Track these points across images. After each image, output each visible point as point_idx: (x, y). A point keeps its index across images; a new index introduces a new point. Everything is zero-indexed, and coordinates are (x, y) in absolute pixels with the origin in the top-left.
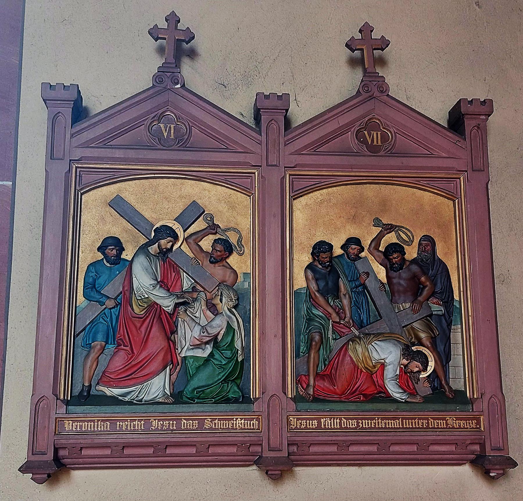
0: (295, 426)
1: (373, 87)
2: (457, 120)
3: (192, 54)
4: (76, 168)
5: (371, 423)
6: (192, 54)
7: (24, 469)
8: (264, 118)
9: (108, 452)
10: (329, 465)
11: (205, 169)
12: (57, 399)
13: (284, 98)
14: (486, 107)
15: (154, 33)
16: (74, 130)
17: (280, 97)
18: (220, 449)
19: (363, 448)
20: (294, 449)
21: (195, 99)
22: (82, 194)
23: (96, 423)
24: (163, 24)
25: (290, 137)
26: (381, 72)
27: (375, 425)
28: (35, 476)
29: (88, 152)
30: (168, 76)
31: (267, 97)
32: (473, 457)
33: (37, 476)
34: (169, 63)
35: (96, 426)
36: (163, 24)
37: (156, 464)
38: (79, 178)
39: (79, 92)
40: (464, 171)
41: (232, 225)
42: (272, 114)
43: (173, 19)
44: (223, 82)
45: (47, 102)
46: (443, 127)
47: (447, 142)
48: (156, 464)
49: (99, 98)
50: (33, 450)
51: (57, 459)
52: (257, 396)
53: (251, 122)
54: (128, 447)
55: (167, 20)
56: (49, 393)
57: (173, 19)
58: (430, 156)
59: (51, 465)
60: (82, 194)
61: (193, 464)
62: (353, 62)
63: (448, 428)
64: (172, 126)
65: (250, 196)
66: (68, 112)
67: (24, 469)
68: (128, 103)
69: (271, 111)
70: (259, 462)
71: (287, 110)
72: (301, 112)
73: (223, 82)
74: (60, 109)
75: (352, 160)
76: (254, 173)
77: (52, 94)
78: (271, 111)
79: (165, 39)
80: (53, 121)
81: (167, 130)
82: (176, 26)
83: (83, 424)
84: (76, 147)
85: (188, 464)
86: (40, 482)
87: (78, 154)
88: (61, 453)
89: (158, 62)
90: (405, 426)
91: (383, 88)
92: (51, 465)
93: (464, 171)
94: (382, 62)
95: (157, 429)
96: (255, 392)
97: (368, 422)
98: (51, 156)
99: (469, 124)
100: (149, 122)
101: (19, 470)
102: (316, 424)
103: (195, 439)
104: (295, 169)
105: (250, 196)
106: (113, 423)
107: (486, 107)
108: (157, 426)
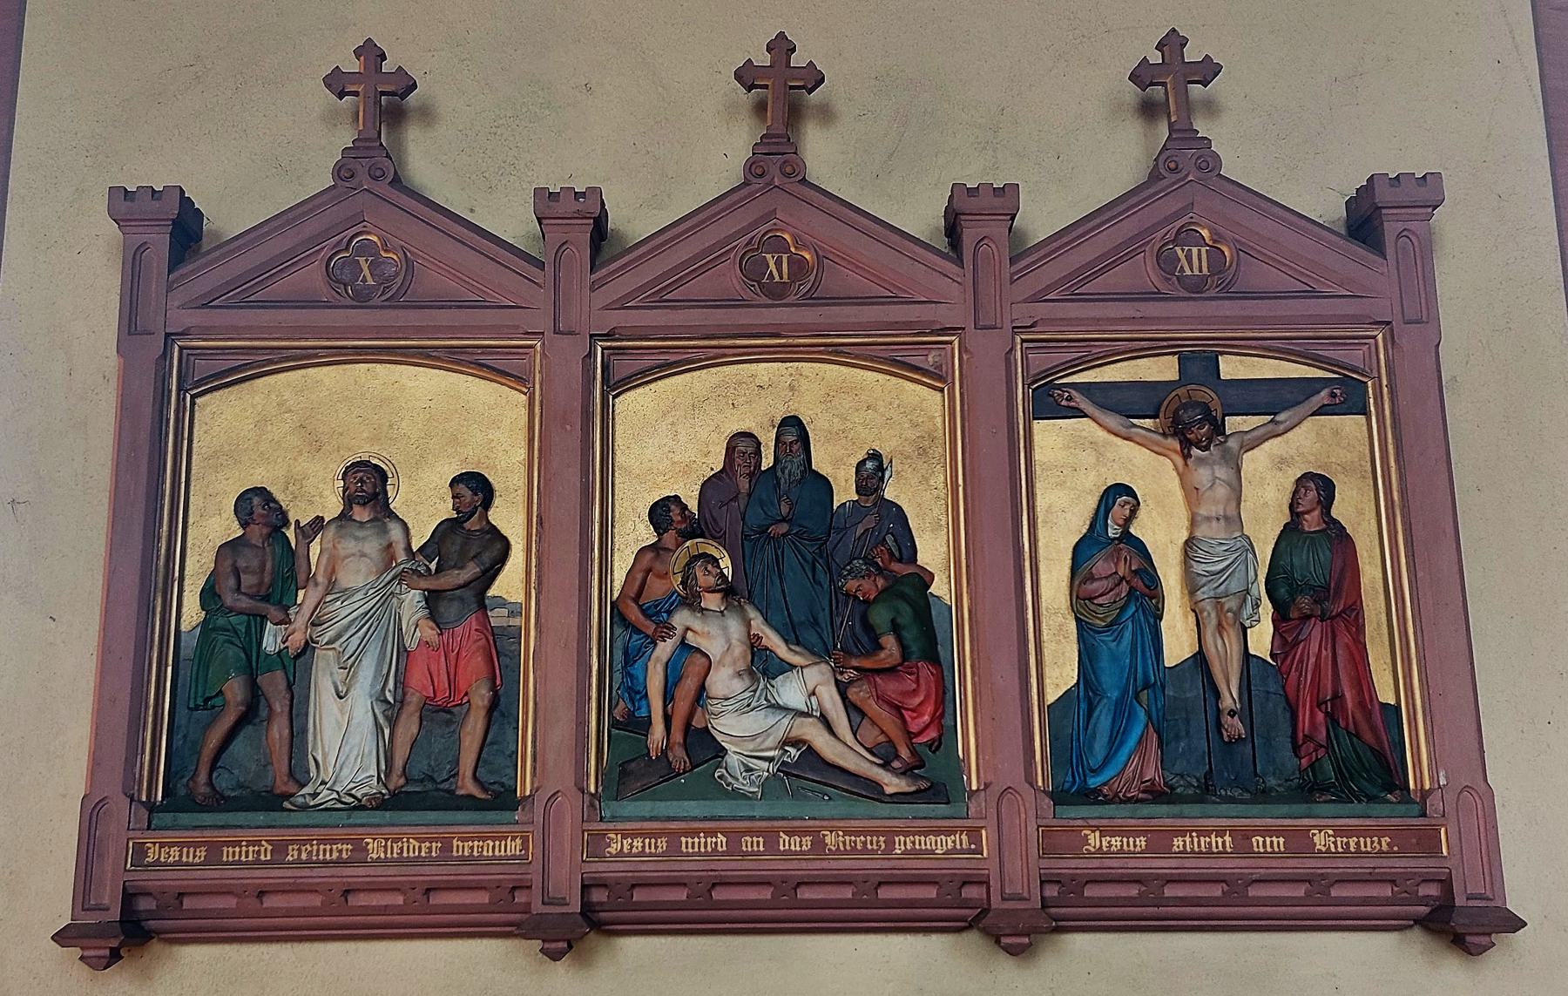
1: (1184, 161)
4: (181, 349)
7: (61, 937)
8: (969, 236)
9: (847, 893)
10: (278, 940)
12: (132, 800)
13: (1009, 192)
14: (1424, 194)
15: (337, 83)
16: (1014, 269)
17: (999, 192)
20: (1052, 891)
21: (835, 206)
26: (1202, 127)
28: (87, 953)
29: (1042, 310)
30: (775, 159)
31: (972, 192)
32: (1424, 910)
33: (553, 945)
34: (366, 140)
42: (567, 229)
43: (781, 46)
47: (1349, 261)
52: (974, 787)
53: (942, 243)
54: (971, 883)
55: (769, 50)
57: (371, 53)
58: (895, 300)
60: (193, 397)
62: (1149, 110)
65: (942, 390)
66: (160, 242)
67: (61, 937)
68: (695, 220)
69: (582, 225)
72: (1041, 217)
73: (880, 170)
74: (985, 231)
76: (951, 343)
78: (974, 217)
79: (766, 87)
81: (1194, 261)
83: (174, 854)
84: (606, 308)
87: (1023, 313)
91: (1209, 163)
92: (122, 925)
96: (525, 786)
105: (942, 390)
107: (1424, 194)
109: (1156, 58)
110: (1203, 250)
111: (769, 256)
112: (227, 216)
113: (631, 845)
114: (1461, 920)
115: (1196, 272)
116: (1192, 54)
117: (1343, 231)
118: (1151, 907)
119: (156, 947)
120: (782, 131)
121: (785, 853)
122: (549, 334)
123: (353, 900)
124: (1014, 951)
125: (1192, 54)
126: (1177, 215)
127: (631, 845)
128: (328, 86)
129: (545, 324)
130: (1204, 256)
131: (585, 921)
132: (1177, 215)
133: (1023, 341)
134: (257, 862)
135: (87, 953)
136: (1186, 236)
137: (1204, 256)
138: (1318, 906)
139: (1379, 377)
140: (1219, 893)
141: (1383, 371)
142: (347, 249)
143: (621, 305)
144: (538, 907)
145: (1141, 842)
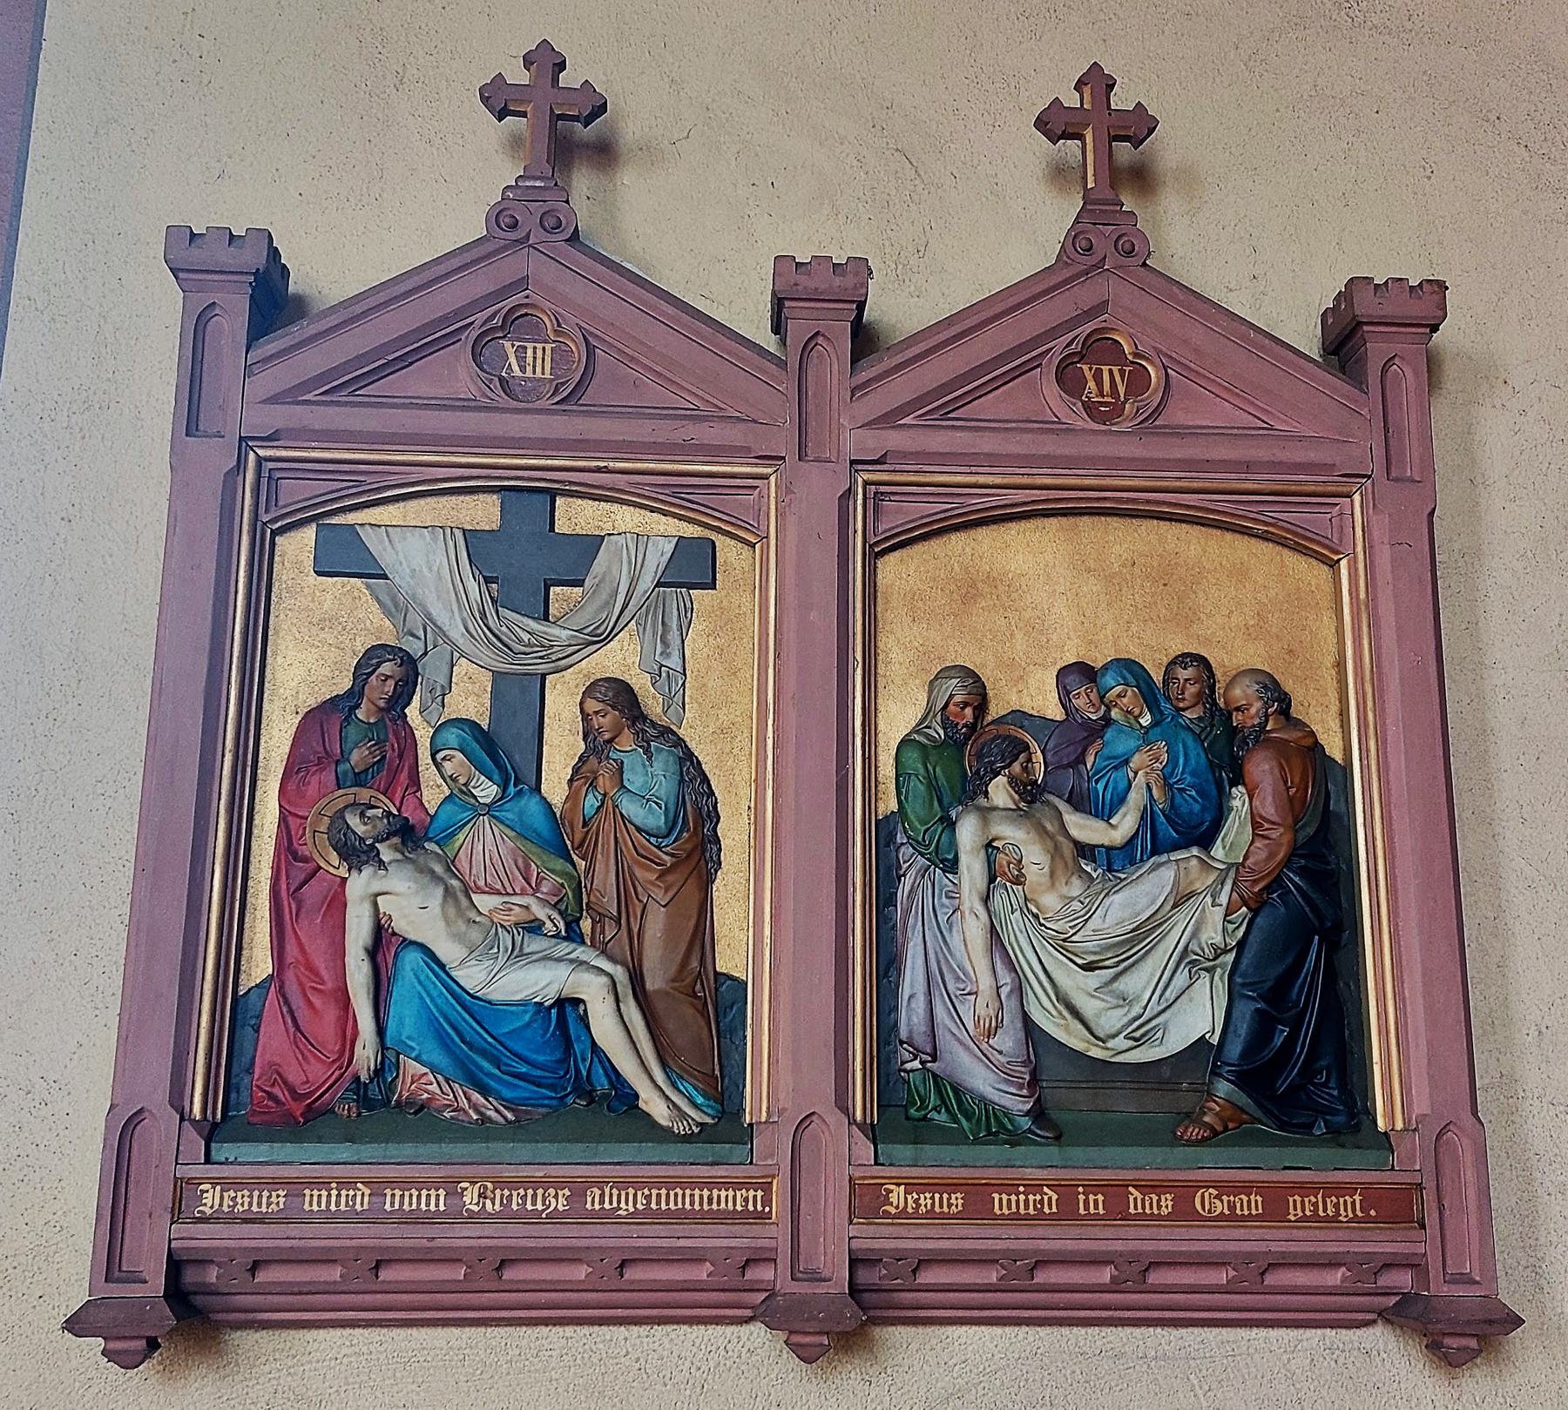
0: (902, 1205)
2: (1345, 339)
3: (604, 153)
5: (735, 1197)
6: (604, 153)
7: (76, 1325)
11: (549, 462)
12: (182, 1119)
14: (1426, 305)
18: (1173, 1273)
19: (1301, 1278)
22: (274, 533)
23: (334, 1192)
24: (519, 76)
25: (864, 376)
27: (649, 1203)
28: (113, 1345)
29: (894, 440)
35: (333, 1199)
36: (519, 76)
37: (961, 1313)
38: (268, 481)
39: (274, 254)
40: (1363, 476)
41: (1165, 661)
44: (703, 233)
45: (181, 275)
46: (1313, 361)
48: (961, 1313)
49: (333, 264)
50: (112, 1262)
51: (178, 1294)
56: (157, 1097)
57: (547, 61)
59: (178, 1308)
60: (274, 533)
61: (1196, 1315)
63: (457, 1216)
64: (548, 347)
67: (76, 1325)
69: (825, 308)
70: (771, 1312)
71: (861, 306)
75: (1050, 446)
77: (197, 256)
78: (825, 308)
79: (524, 115)
80: (199, 329)
82: (555, 80)
83: (240, 1198)
85: (1083, 1314)
86: (126, 1361)
88: (190, 1277)
89: (509, 172)
90: (1092, 1211)
92: (178, 1308)
93: (1363, 476)
94: (1142, 178)
95: (903, 1214)
97: (1009, 1201)
98: (191, 420)
99: (1376, 350)
100: (475, 334)
101: (1519, 1322)
102: (960, 1202)
103: (876, 1244)
104: (879, 467)
105: (753, 546)
106: (578, 1190)
107: (1426, 305)
108: (217, 1201)
109: (1071, 100)
110: (548, 347)
111: (507, 345)
112: (326, 270)
113: (916, 1201)
114: (1463, 1329)
115: (529, 374)
116: (1121, 100)
117: (1312, 348)
118: (374, 1287)
119: (246, 1341)
120: (1108, 194)
121: (1137, 1217)
122: (792, 458)
123: (632, 1274)
124: (807, 1355)
125: (1121, 100)
126: (1090, 314)
127: (916, 1201)
128: (485, 100)
129: (784, 444)
130: (548, 352)
131: (850, 1315)
132: (1090, 314)
133: (866, 483)
134: (1040, 1216)
135: (113, 1345)
136: (515, 323)
137: (548, 352)
138: (621, 1292)
139: (1355, 557)
140: (1107, 1279)
141: (1359, 548)
142: (1136, 355)
143: (888, 420)
144: (786, 1285)
145: (957, 1199)
